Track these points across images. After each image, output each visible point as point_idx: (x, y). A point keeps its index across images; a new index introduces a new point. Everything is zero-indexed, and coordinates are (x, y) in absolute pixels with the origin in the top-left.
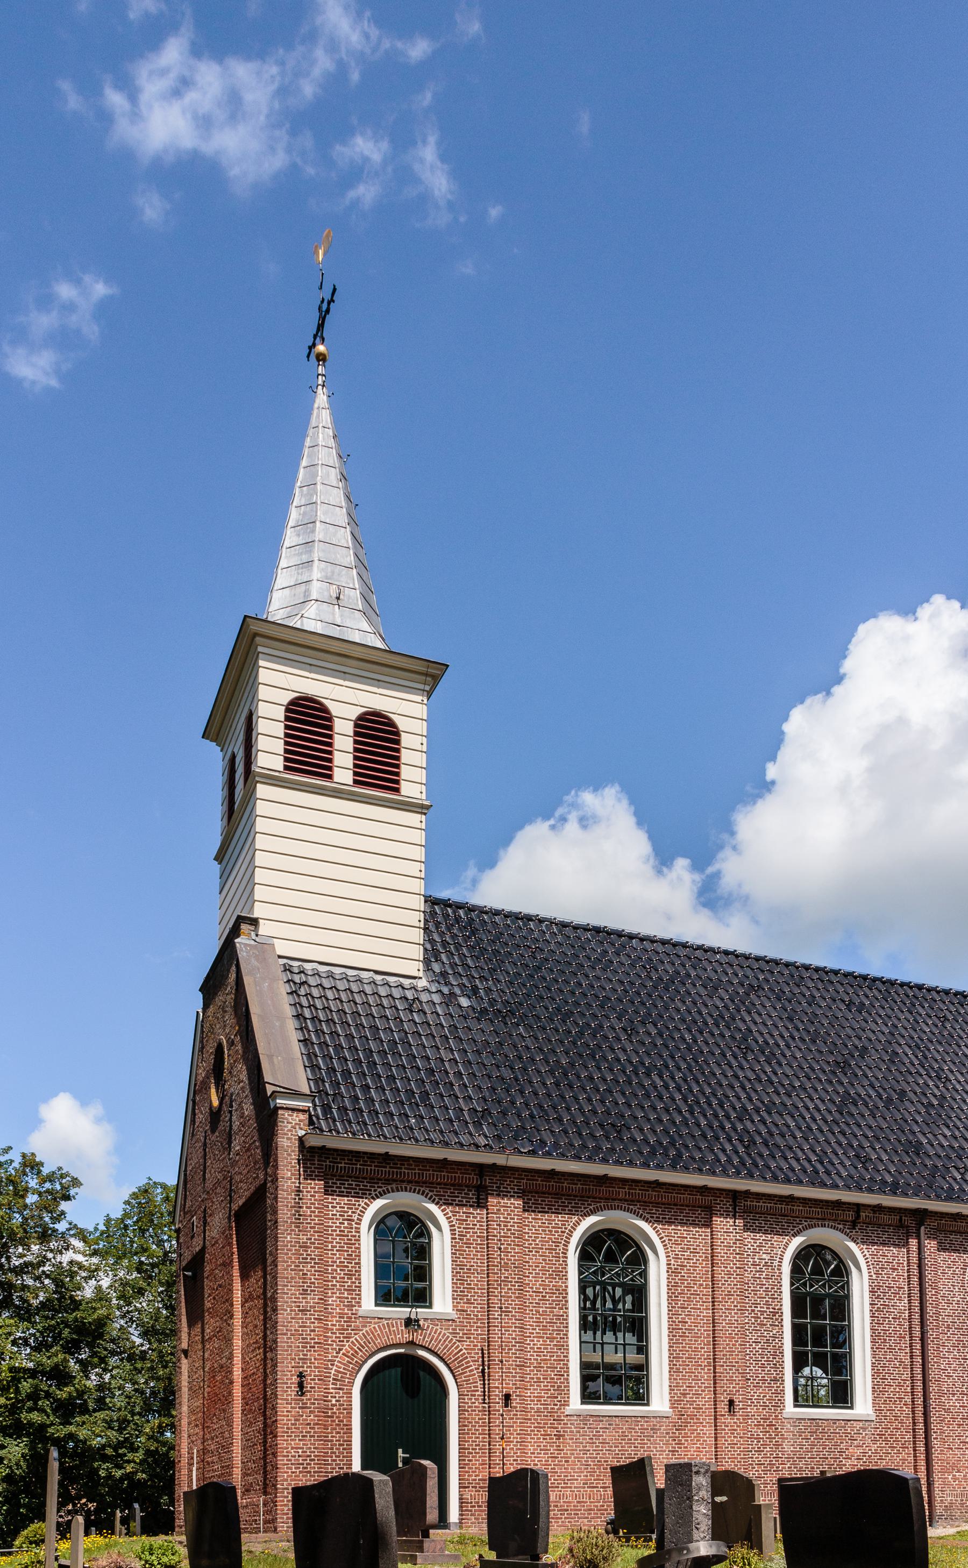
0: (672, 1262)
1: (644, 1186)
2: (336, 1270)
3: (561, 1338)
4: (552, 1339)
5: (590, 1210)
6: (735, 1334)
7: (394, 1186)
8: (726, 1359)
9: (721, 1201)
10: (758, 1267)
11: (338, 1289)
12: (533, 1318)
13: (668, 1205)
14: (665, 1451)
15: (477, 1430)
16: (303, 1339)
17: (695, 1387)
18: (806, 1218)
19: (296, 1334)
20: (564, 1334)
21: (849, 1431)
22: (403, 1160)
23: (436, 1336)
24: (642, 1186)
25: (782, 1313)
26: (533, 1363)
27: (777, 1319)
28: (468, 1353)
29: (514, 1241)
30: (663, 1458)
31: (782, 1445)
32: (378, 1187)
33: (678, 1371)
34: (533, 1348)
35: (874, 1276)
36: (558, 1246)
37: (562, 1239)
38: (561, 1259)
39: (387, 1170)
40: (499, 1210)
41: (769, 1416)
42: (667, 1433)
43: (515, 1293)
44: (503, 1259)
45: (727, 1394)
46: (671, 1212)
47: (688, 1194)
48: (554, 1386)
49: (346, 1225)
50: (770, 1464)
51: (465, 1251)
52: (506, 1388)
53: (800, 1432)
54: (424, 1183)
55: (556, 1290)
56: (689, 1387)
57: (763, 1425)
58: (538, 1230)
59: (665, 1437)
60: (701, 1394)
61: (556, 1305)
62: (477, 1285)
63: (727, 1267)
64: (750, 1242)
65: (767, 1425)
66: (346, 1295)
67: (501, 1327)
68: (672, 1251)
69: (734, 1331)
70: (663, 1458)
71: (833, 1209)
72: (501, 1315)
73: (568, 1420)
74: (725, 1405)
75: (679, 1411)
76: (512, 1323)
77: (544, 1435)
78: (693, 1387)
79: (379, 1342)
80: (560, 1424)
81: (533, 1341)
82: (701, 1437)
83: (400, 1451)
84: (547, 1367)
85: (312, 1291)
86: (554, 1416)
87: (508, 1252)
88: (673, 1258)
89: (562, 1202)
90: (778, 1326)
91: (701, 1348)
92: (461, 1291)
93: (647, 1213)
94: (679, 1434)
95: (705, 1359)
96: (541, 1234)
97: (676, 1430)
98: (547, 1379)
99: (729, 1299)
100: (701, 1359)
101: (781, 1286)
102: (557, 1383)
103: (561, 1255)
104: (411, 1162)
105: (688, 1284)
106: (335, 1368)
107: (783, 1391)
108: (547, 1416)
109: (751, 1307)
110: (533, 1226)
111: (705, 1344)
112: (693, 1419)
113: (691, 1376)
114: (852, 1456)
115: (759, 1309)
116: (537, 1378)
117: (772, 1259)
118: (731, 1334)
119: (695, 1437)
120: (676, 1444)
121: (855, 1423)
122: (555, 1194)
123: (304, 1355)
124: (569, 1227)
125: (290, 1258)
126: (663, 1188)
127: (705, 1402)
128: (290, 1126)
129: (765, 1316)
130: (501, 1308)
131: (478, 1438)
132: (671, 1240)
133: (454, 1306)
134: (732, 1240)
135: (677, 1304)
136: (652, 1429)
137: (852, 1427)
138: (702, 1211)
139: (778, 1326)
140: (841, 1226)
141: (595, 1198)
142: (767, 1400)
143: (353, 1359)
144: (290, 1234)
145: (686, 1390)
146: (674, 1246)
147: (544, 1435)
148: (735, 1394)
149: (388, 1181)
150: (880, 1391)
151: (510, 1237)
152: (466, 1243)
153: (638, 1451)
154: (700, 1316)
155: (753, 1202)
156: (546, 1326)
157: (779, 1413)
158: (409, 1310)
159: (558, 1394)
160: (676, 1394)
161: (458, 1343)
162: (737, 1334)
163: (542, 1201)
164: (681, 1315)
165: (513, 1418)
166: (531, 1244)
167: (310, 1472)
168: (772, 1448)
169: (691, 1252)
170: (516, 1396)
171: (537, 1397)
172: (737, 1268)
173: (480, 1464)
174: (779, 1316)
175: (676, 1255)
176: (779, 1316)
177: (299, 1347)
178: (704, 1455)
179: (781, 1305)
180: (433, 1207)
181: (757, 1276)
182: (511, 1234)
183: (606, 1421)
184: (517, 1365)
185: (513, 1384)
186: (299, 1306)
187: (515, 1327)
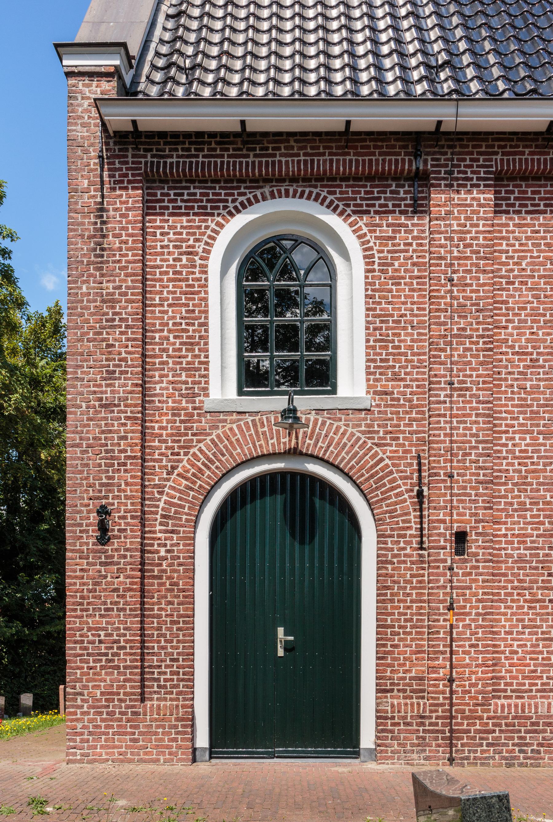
2: (167, 338)
7: (267, 190)
12: (513, 399)
15: (409, 595)
16: (107, 451)
23: (337, 438)
28: (394, 465)
29: (477, 265)
32: (240, 194)
34: (512, 452)
43: (477, 356)
49: (184, 261)
51: (391, 291)
52: (458, 521)
58: (526, 245)
66: (184, 378)
67: (451, 416)
72: (451, 396)
76: (472, 409)
79: (239, 454)
81: (513, 439)
83: (281, 631)
84: (539, 484)
85: (121, 373)
87: (466, 285)
92: (382, 360)
96: (531, 251)
98: (537, 503)
104: (292, 143)
106: (165, 497)
108: (536, 568)
110: (516, 239)
116: (519, 503)
123: (109, 478)
130: (451, 383)
131: (409, 608)
133: (369, 386)
144: (87, 282)
152: (392, 278)
156: (538, 412)
161: (376, 448)
163: (533, 192)
165: (470, 574)
166: (512, 270)
171: (518, 536)
173: (412, 653)
177: (100, 465)
182: (472, 252)
184: (478, 482)
186: (101, 399)
187: (477, 415)
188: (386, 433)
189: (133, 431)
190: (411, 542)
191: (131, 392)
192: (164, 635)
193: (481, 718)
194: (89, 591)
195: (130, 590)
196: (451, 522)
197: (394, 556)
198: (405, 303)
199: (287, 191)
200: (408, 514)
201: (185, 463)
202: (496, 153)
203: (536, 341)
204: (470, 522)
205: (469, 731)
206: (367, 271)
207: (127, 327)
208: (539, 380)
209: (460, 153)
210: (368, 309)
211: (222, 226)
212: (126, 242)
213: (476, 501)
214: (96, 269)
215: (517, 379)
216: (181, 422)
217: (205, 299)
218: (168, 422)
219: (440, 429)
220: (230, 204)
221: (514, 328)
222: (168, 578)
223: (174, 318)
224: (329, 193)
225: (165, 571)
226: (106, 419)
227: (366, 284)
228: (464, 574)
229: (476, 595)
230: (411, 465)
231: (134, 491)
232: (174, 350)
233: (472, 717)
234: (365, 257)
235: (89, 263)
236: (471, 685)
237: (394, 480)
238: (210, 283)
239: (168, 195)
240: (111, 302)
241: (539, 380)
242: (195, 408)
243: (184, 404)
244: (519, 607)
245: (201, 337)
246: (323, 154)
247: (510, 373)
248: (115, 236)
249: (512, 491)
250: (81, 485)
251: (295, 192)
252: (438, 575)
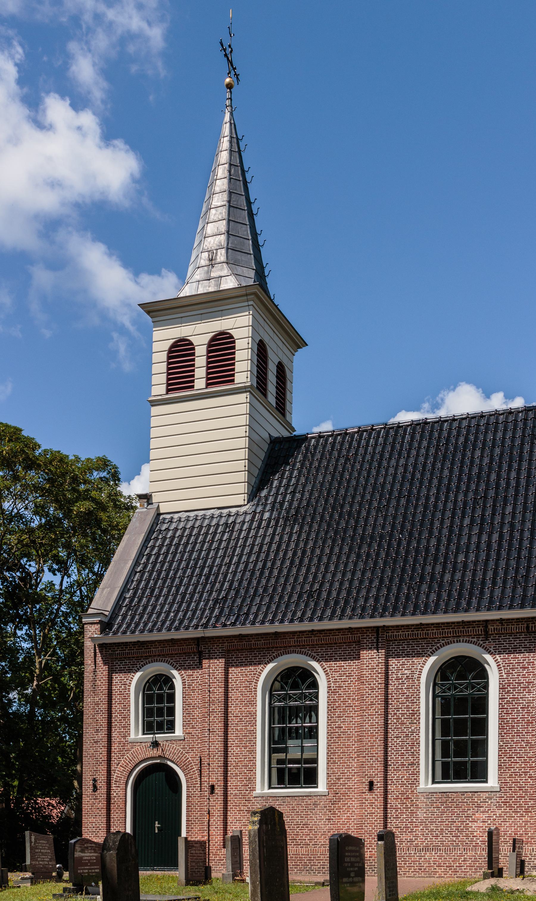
0: (332, 685)
1: (308, 635)
2: (117, 716)
4: (245, 747)
5: (274, 656)
7: (150, 660)
8: (368, 751)
10: (400, 681)
12: (233, 734)
13: (329, 645)
14: (323, 819)
15: (197, 809)
16: (96, 758)
17: (347, 773)
18: (443, 637)
19: (93, 756)
20: (254, 743)
21: (476, 800)
23: (173, 751)
24: (306, 635)
25: (419, 713)
26: (233, 764)
27: (415, 719)
28: (192, 760)
29: (218, 685)
30: (321, 824)
31: (416, 813)
32: (141, 662)
33: (334, 762)
34: (233, 754)
35: (505, 676)
36: (251, 684)
37: (254, 679)
39: (390, 634)
41: (406, 791)
43: (218, 719)
46: (332, 649)
47: (341, 635)
48: (246, 778)
49: (123, 688)
50: (405, 827)
51: (191, 695)
53: (432, 803)
55: (249, 714)
56: (342, 773)
57: (401, 799)
59: (323, 809)
60: (352, 778)
63: (370, 684)
64: (395, 663)
66: (122, 730)
67: (209, 742)
68: (332, 677)
69: (375, 730)
70: (321, 824)
71: (464, 628)
72: (209, 734)
73: (255, 800)
74: (365, 785)
75: (334, 791)
76: (216, 739)
77: (239, 811)
78: (346, 773)
79: (141, 757)
80: (250, 803)
82: (351, 809)
83: (157, 822)
84: (242, 766)
85: (101, 730)
86: (246, 798)
87: (215, 693)
88: (333, 682)
90: (416, 723)
91: (353, 745)
92: (188, 721)
93: (314, 652)
94: (334, 807)
95: (355, 753)
96: (240, 677)
97: (332, 804)
99: (371, 707)
100: (352, 752)
102: (248, 776)
103: (253, 690)
105: (343, 699)
106: (116, 774)
107: (419, 772)
108: (241, 798)
109: (394, 711)
110: (235, 673)
111: (355, 742)
112: (345, 796)
113: (344, 766)
115: (400, 712)
116: (235, 774)
117: (413, 673)
118: (373, 733)
120: (331, 814)
121: (482, 794)
123: (96, 768)
124: (259, 670)
125: (90, 712)
127: (355, 783)
128: (90, 633)
129: (406, 716)
130: (209, 730)
131: (197, 814)
132: (332, 669)
133: (184, 731)
135: (335, 715)
136: (313, 804)
137: (479, 797)
138: (356, 645)
139: (416, 723)
140: (475, 640)
141: (277, 647)
143: (125, 769)
144: (90, 697)
145: (340, 776)
146: (333, 673)
147: (239, 811)
148: (375, 777)
149: (147, 657)
150: (506, 768)
151: (216, 683)
152: (192, 690)
153: (303, 819)
154: (352, 722)
156: (242, 739)
157: (414, 789)
158: (152, 736)
160: (332, 779)
161: (186, 754)
162: (378, 733)
163: (241, 655)
166: (233, 685)
167: (99, 836)
168: (408, 815)
169: (346, 676)
170: (218, 786)
171: (235, 786)
174: (417, 716)
175: (335, 679)
176: (417, 716)
179: (419, 708)
180: (315, 664)
181: (400, 687)
182: (217, 680)
183: (281, 800)
186: (94, 740)
187: (218, 741)
188: (190, 748)
189: (104, 751)
190: (197, 789)
191: (104, 737)
192: (115, 825)
193: (219, 855)
197: (192, 794)
198: (196, 699)
199: (157, 659)
200: (197, 778)
201: (122, 761)
203: (242, 711)
206: (183, 688)
208: (242, 726)
209: (213, 644)
210: (183, 702)
211: (134, 676)
212: (102, 683)
215: (235, 726)
216: (122, 746)
217: (129, 701)
218: (117, 746)
219: (205, 747)
220: (138, 666)
221: (234, 707)
223: (119, 708)
224: (171, 659)
225: (116, 801)
226: (95, 747)
227: (183, 693)
229: (217, 809)
230: (198, 760)
231: (104, 773)
232: (120, 720)
234: (183, 683)
235: (91, 691)
236: (216, 843)
238: (131, 695)
240: (97, 704)
241: (242, 726)
243: (122, 740)
244: (235, 813)
246: (167, 647)
247: (232, 724)
248: (99, 681)
249: (233, 769)
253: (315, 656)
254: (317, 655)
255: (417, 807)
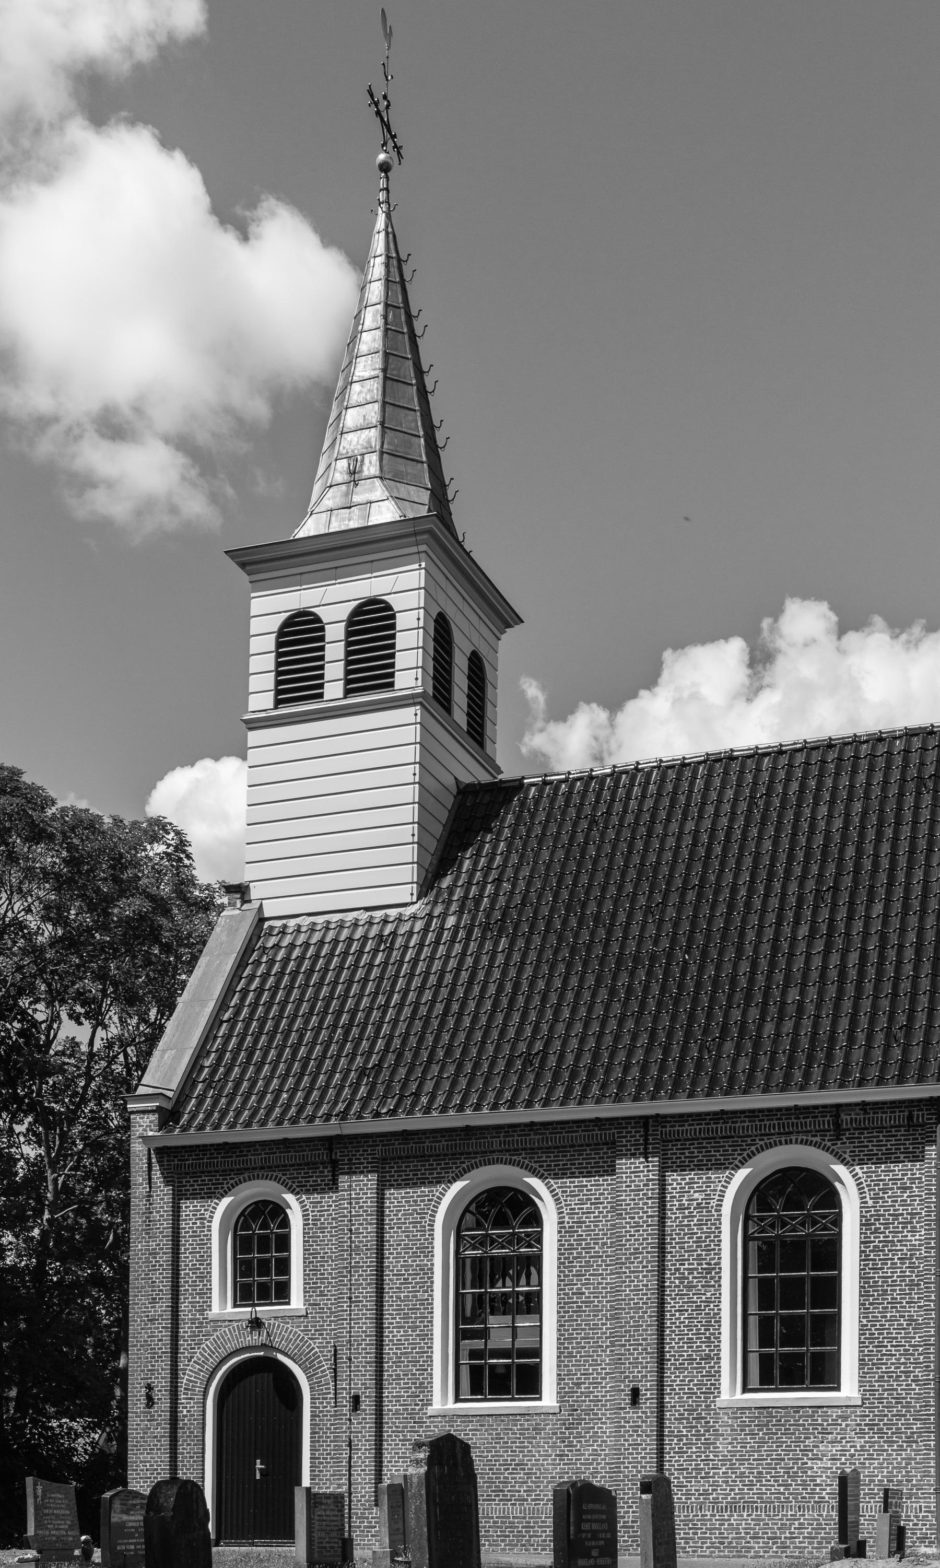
0: (567, 1219)
1: (524, 1130)
2: (188, 1274)
3: (424, 1326)
4: (414, 1328)
6: (643, 1303)
7: (246, 1175)
8: (630, 1336)
9: (627, 1132)
10: (686, 1211)
11: (191, 1294)
12: (392, 1306)
14: (551, 1456)
16: (151, 1349)
17: (592, 1374)
20: (428, 1322)
21: (820, 1422)
22: (249, 1147)
25: (720, 1268)
26: (392, 1358)
27: (712, 1278)
29: (366, 1220)
30: (548, 1464)
32: (231, 1179)
34: (392, 1341)
35: (870, 1203)
36: (424, 1218)
37: (428, 1209)
38: (428, 1233)
40: (350, 1186)
42: (555, 1433)
43: (366, 1280)
44: (354, 1242)
45: (629, 1381)
46: (566, 1156)
47: (583, 1131)
48: (415, 1383)
49: (198, 1224)
51: (319, 1237)
52: (354, 1389)
53: (743, 1427)
54: (276, 1167)
55: (421, 1270)
56: (584, 1374)
57: (688, 1419)
58: (401, 1202)
59: (551, 1438)
60: (601, 1383)
61: (420, 1287)
62: (331, 1274)
65: (693, 1419)
67: (351, 1319)
68: (566, 1205)
69: (642, 1299)
70: (548, 1464)
72: (350, 1306)
75: (570, 1406)
76: (363, 1314)
79: (230, 1347)
80: (422, 1427)
81: (392, 1332)
82: (599, 1437)
83: (258, 1461)
84: (408, 1362)
85: (160, 1299)
86: (415, 1418)
88: (567, 1214)
89: (430, 1165)
91: (603, 1324)
92: (314, 1283)
93: (535, 1162)
94: (570, 1433)
95: (607, 1338)
96: (404, 1206)
97: (566, 1429)
98: (407, 1375)
99: (635, 1258)
100: (601, 1338)
101: (720, 1232)
104: (258, 1147)
108: (406, 1418)
109: (675, 1265)
110: (395, 1198)
111: (607, 1319)
112: (589, 1414)
113: (588, 1361)
114: (824, 1455)
115: (687, 1266)
116: (396, 1375)
117: (708, 1197)
119: (590, 1437)
120: (565, 1446)
122: (421, 1157)
126: (548, 1129)
127: (606, 1392)
130: (350, 1298)
131: (329, 1446)
133: (306, 1300)
134: (643, 1181)
135: (572, 1271)
136: (534, 1429)
137: (825, 1417)
138: (608, 1149)
139: (714, 1286)
140: (818, 1139)
142: (694, 1385)
145: (580, 1379)
146: (569, 1198)
149: (240, 1172)
150: (873, 1364)
151: (362, 1215)
152: (320, 1228)
154: (602, 1283)
155: (709, 1124)
158: (249, 1309)
159: (420, 1392)
162: (647, 1303)
163: (406, 1167)
164: (576, 1284)
165: (361, 1423)
166: (393, 1220)
168: (700, 1448)
169: (591, 1204)
170: (366, 1397)
171: (395, 1397)
172: (647, 1217)
173: (331, 1475)
174: (716, 1273)
175: (571, 1209)
176: (716, 1273)
177: (147, 1358)
178: (602, 1460)
179: (720, 1258)
180: (535, 1183)
181: (686, 1223)
182: (364, 1211)
183: (477, 1421)
184: (366, 1362)
185: (362, 1384)
186: (148, 1316)
187: (366, 1318)
188: (316, 1331)
189: (166, 1336)
193: (367, 1518)
194: (141, 1438)
195: (164, 1437)
196: (350, 1389)
197: (320, 1412)
199: (258, 1175)
200: (329, 1384)
202: (378, 1145)
204: (361, 1389)
205: (360, 1527)
206: (304, 1225)
207: (163, 1270)
210: (305, 1250)
211: (217, 1204)
213: (365, 1375)
214: (146, 1234)
215: (395, 1292)
216: (196, 1327)
217: (210, 1248)
218: (189, 1328)
219: (344, 1328)
222: (189, 1428)
224: (284, 1175)
225: (186, 1424)
228: (358, 1423)
229: (365, 1436)
230: (330, 1351)
231: (166, 1374)
233: (363, 1517)
234: (303, 1216)
236: (362, 1496)
237: (320, 1362)
239: (189, 1182)
240: (154, 1254)
242: (204, 1319)
245: (208, 1273)
246: (275, 1153)
250: (137, 1371)
251: (263, 1175)
252: (342, 1424)
253: (536, 1169)
254: (540, 1166)
255: (717, 1435)
